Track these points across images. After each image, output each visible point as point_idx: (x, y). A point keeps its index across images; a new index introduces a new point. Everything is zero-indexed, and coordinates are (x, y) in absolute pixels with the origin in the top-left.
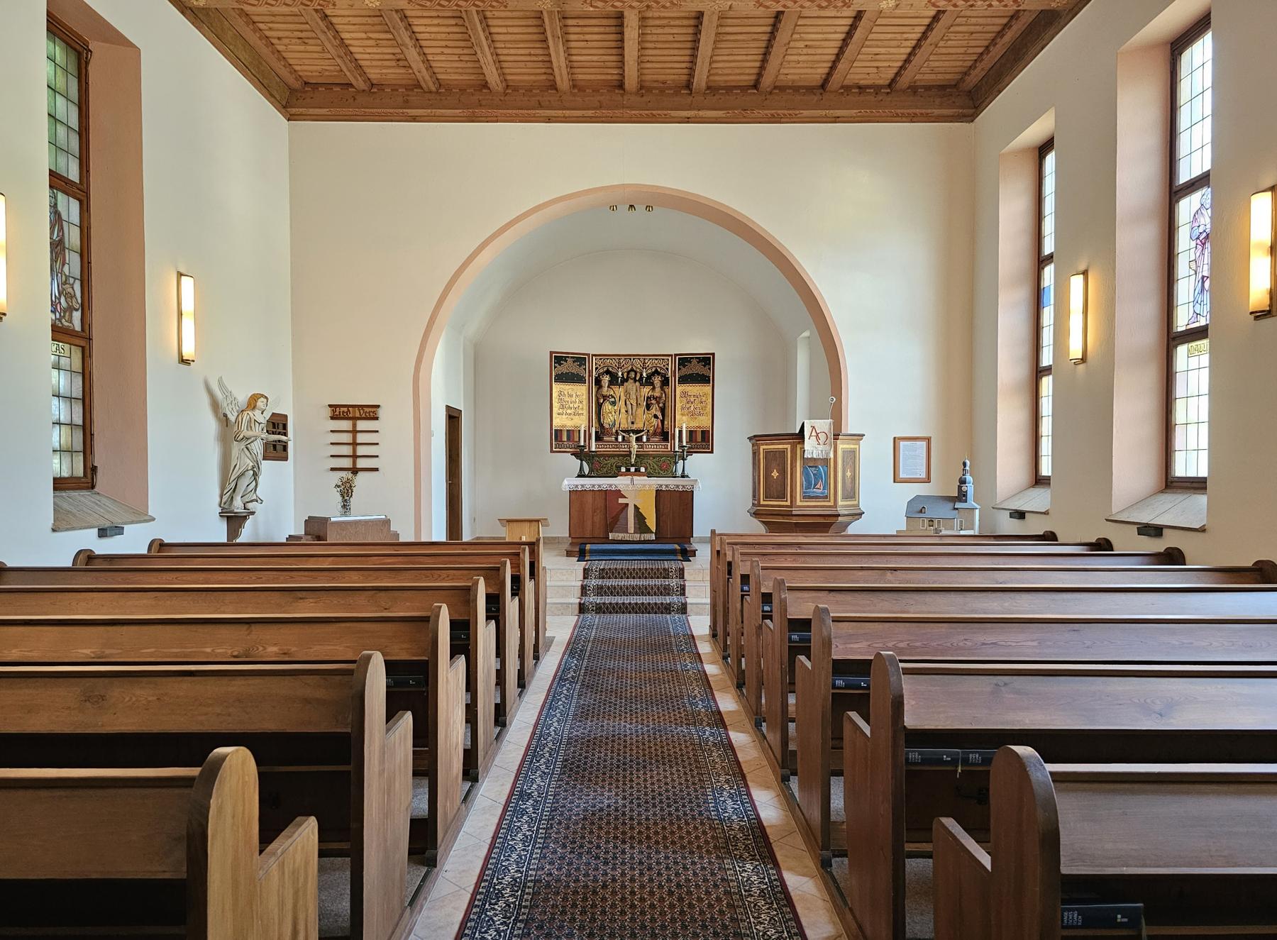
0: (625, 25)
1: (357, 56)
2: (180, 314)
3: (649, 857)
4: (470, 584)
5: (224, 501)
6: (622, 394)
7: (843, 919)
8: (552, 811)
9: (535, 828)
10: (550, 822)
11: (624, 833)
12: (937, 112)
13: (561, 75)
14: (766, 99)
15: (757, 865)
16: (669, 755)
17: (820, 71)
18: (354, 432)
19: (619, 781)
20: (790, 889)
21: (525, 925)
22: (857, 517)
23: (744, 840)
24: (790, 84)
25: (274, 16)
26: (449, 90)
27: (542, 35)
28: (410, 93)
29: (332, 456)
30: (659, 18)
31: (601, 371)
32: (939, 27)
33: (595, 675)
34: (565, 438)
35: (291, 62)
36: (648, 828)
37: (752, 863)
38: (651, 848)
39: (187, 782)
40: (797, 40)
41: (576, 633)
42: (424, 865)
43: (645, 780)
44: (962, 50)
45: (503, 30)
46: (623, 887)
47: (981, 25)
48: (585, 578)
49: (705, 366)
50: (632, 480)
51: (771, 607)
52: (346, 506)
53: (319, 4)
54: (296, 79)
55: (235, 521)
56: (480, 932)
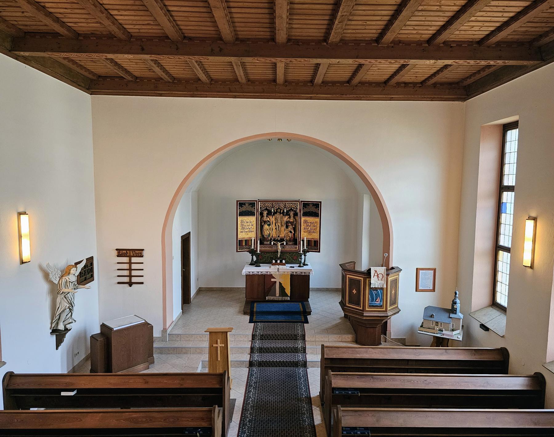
2: (20, 237)
6: (274, 220)
14: (354, 89)
34: (244, 244)
49: (316, 208)
54: (93, 75)
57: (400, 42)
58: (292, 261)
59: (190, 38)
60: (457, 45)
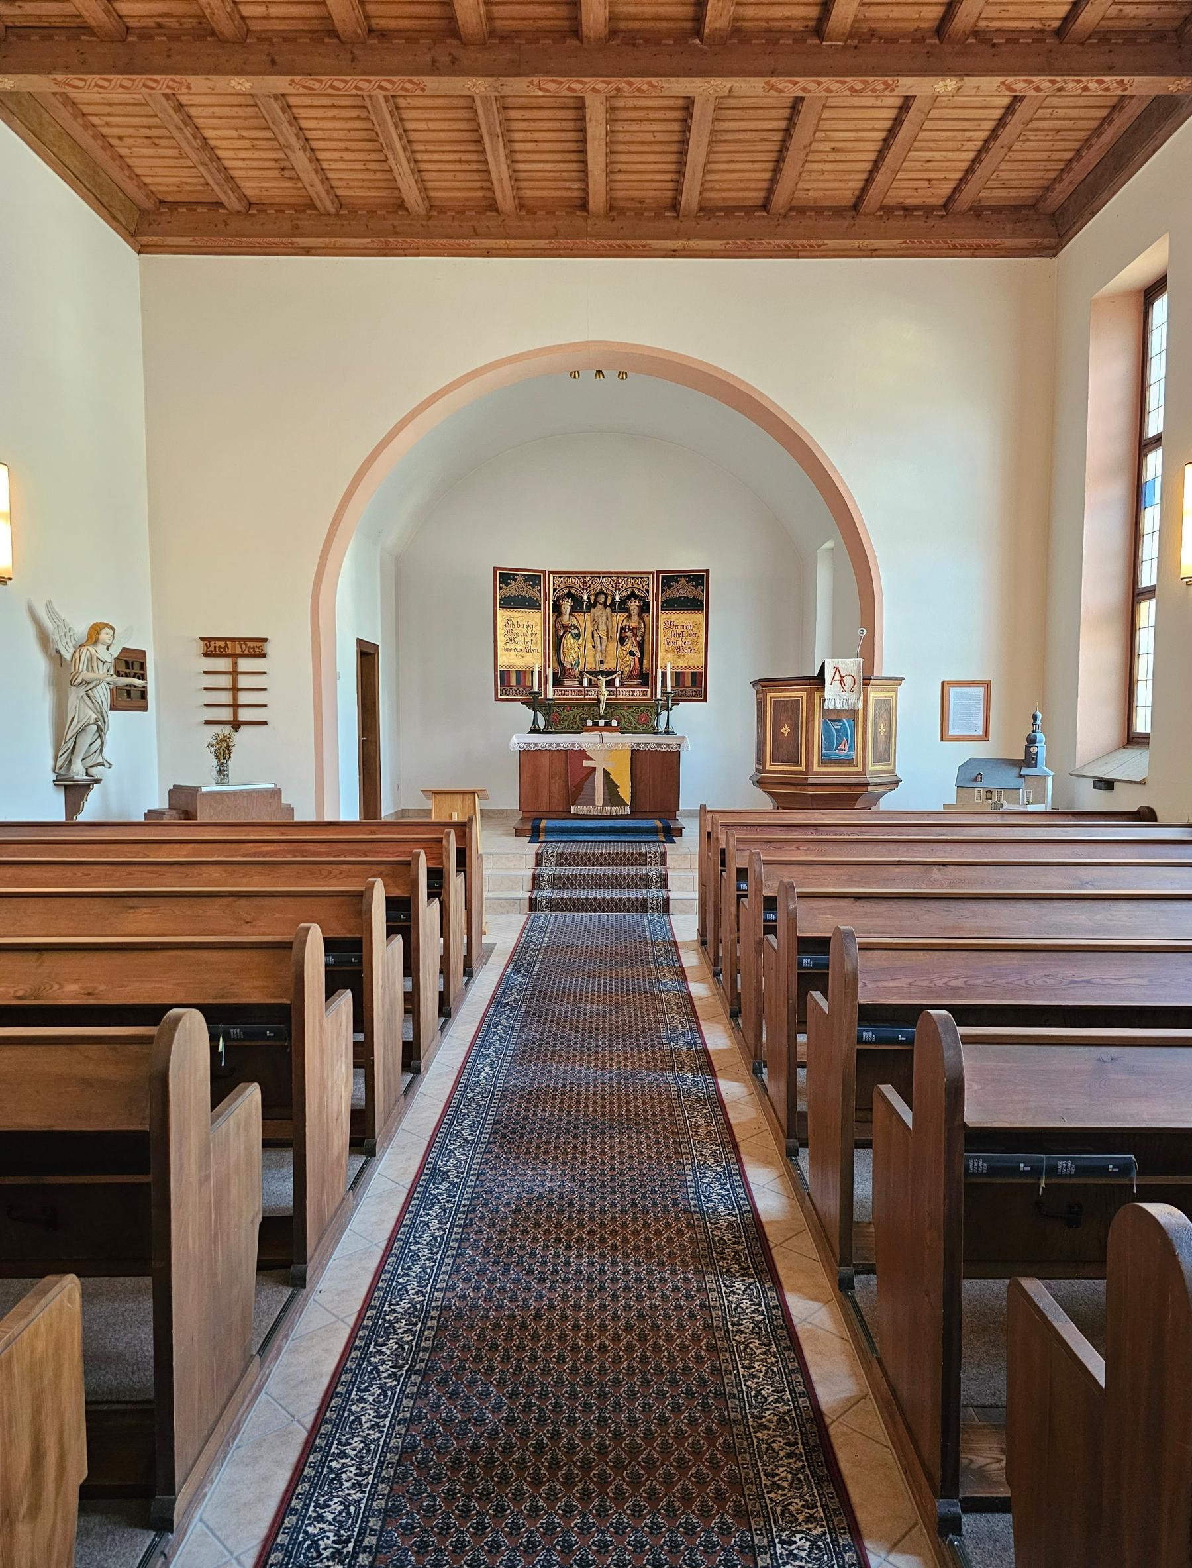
0: (587, 118)
1: (227, 163)
3: (602, 1272)
4: (363, 889)
5: (59, 764)
6: (588, 624)
7: (868, 1372)
8: (473, 1199)
9: (448, 1226)
10: (470, 1216)
11: (569, 1233)
12: (1008, 242)
13: (503, 190)
15: (750, 1284)
16: (637, 1115)
17: (852, 185)
18: (235, 673)
19: (567, 1153)
20: (796, 1321)
21: (423, 1378)
22: (891, 787)
23: (734, 1243)
24: (811, 204)
25: (110, 105)
26: (353, 211)
27: (476, 134)
28: (302, 216)
29: (205, 705)
30: (635, 108)
31: (561, 593)
32: (1015, 121)
33: (544, 998)
34: (513, 682)
35: (139, 171)
36: (602, 1226)
37: (743, 1281)
38: (605, 1256)
39: (147, 1040)
40: (821, 141)
41: (523, 939)
42: (288, 1286)
43: (603, 1152)
44: (1044, 156)
45: (422, 125)
46: (563, 1317)
47: (1071, 119)
48: (537, 865)
49: (696, 587)
50: (601, 737)
51: (775, 914)
52: (222, 772)
53: (168, 87)
54: (147, 196)
55: (75, 791)
56: (359, 1390)
57: (873, 33)
58: (636, 728)
59: (382, 34)
60: (1008, 41)
